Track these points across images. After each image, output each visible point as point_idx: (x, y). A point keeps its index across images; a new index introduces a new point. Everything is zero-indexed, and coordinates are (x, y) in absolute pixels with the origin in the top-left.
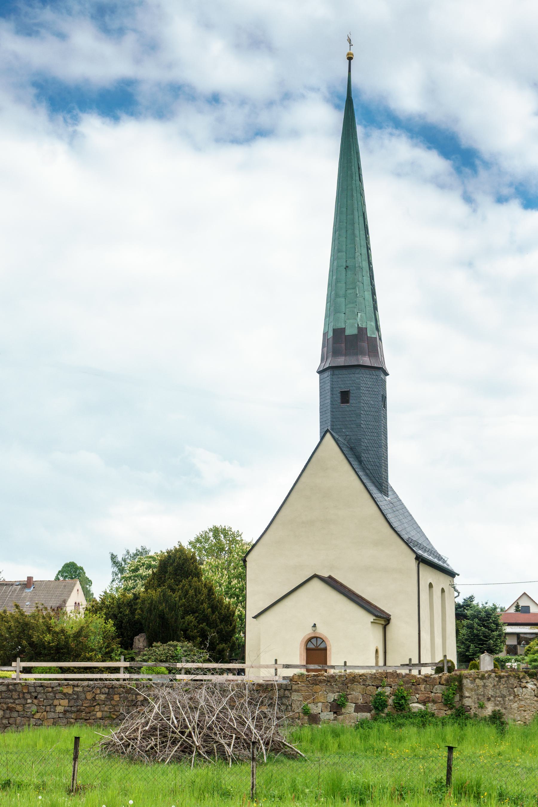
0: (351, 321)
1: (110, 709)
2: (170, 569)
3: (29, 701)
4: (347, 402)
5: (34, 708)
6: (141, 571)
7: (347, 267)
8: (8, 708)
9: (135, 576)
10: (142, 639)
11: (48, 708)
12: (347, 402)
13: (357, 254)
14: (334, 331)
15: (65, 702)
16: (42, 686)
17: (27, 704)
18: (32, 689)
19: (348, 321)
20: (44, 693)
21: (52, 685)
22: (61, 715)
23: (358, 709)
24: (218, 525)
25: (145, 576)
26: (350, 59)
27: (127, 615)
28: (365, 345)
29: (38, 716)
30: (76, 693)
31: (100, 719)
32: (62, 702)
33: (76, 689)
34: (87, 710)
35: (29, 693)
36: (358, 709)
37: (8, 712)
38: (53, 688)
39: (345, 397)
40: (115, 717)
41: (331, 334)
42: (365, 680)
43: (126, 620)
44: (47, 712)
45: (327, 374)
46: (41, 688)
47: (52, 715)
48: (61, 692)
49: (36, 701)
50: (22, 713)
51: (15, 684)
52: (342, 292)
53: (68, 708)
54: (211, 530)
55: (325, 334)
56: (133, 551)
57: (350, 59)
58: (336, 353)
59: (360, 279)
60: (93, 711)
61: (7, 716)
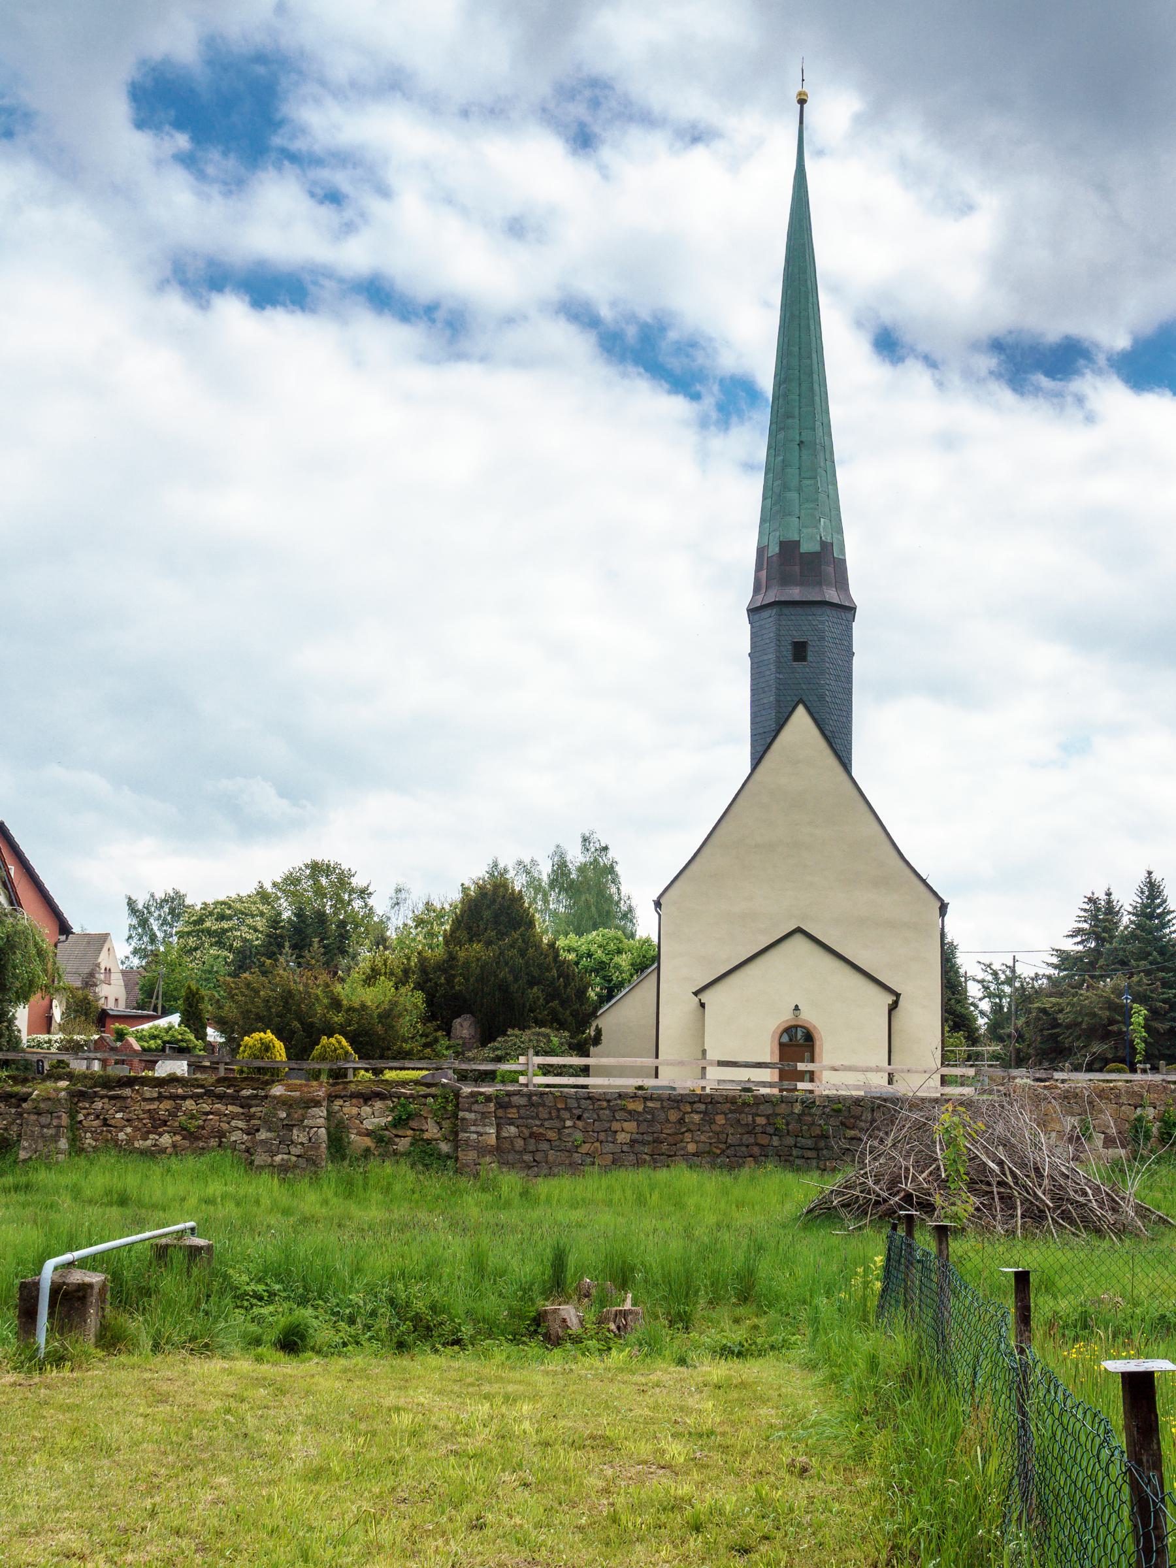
0: (810, 530)
1: (710, 1138)
2: (487, 914)
3: (569, 1123)
4: (804, 659)
5: (579, 1136)
6: (208, 924)
7: (802, 442)
8: (532, 1135)
9: (198, 931)
10: (466, 1024)
11: (602, 1136)
12: (804, 659)
13: (818, 423)
14: (782, 544)
15: (631, 1126)
16: (589, 1098)
17: (565, 1128)
18: (573, 1103)
19: (804, 530)
20: (593, 1110)
21: (608, 1097)
22: (625, 1148)
23: (1109, 1142)
24: (319, 859)
25: (215, 931)
26: (802, 102)
27: (441, 985)
28: (831, 569)
29: (585, 1148)
30: (651, 1111)
31: (694, 1155)
32: (625, 1125)
33: (650, 1104)
34: (671, 1140)
35: (567, 1109)
36: (1109, 1142)
37: (533, 1141)
38: (609, 1101)
39: (800, 651)
40: (718, 1152)
41: (774, 549)
42: (1118, 1096)
43: (441, 991)
44: (601, 1142)
45: (766, 614)
46: (588, 1102)
47: (610, 1147)
48: (624, 1109)
49: (580, 1124)
50: (557, 1143)
51: (542, 1094)
52: (794, 483)
53: (637, 1136)
54: (307, 866)
55: (761, 551)
56: (160, 895)
57: (802, 102)
58: (785, 580)
59: (822, 464)
60: (682, 1141)
61: (531, 1148)
